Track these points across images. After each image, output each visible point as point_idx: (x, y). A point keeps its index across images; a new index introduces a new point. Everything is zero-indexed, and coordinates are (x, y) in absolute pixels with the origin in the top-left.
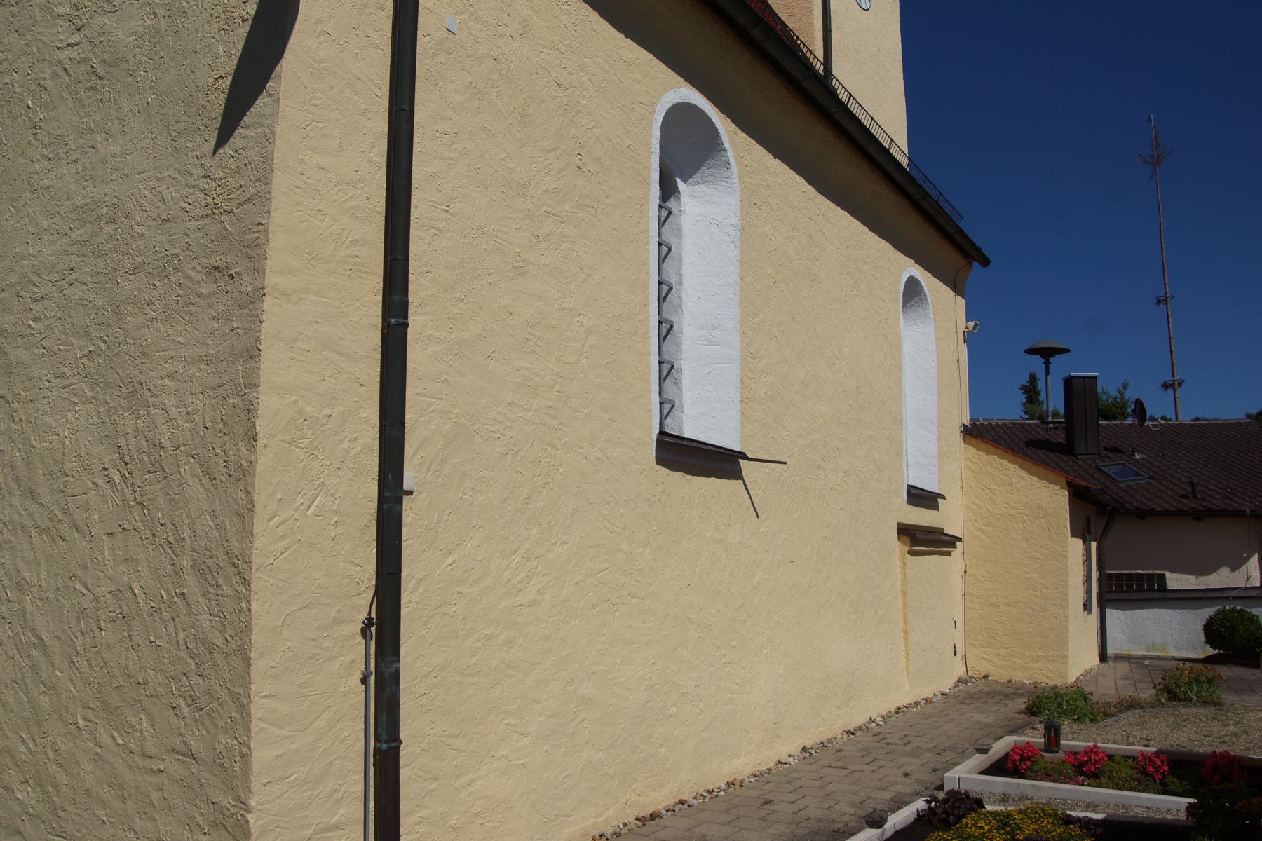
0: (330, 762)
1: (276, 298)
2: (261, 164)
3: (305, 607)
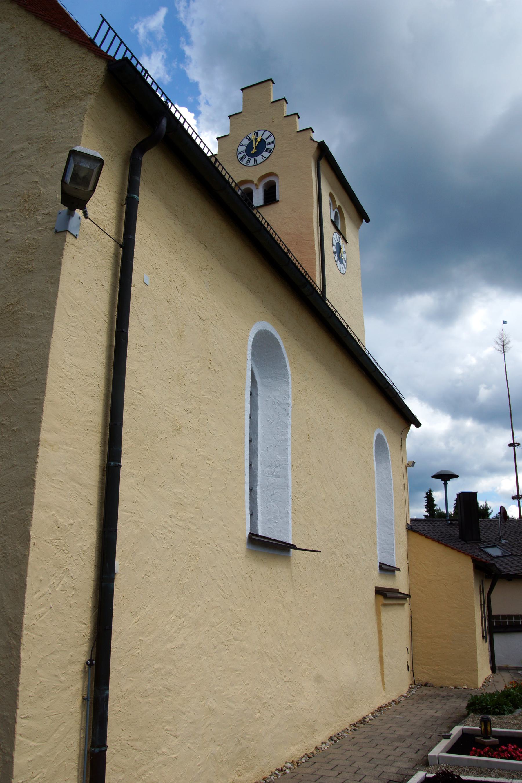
0: (61, 764)
1: (46, 447)
2: (39, 362)
3: (52, 653)
